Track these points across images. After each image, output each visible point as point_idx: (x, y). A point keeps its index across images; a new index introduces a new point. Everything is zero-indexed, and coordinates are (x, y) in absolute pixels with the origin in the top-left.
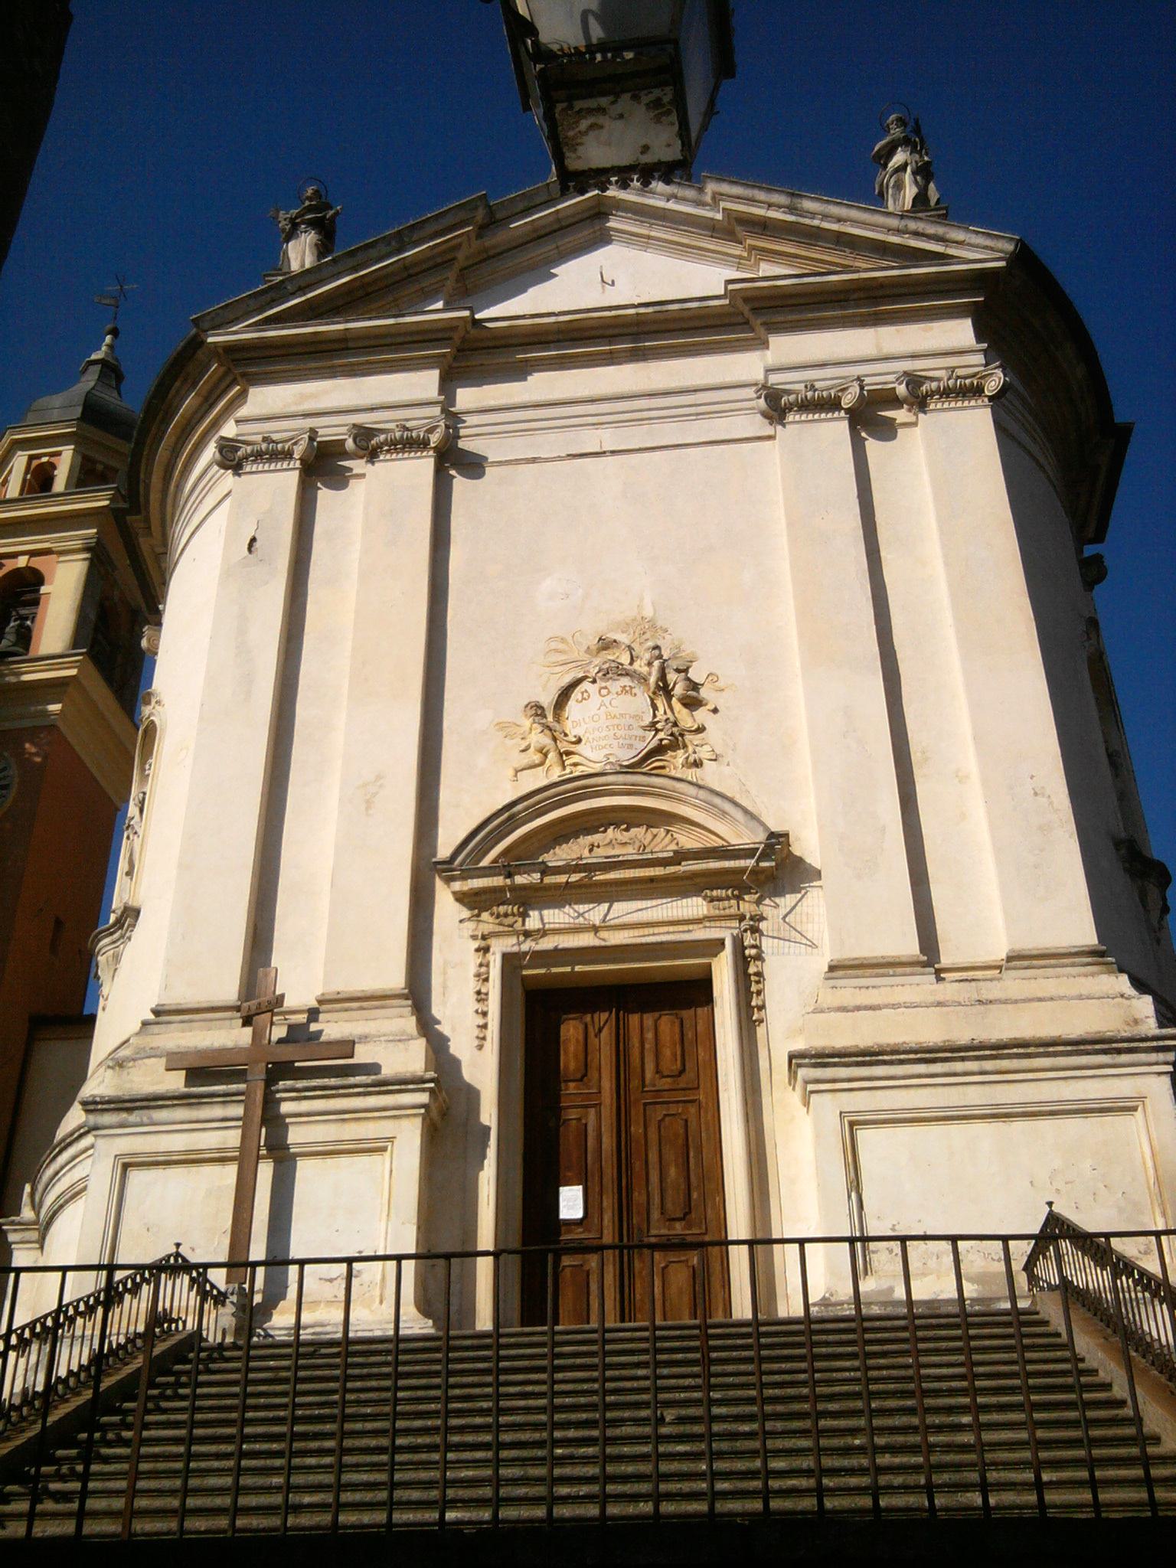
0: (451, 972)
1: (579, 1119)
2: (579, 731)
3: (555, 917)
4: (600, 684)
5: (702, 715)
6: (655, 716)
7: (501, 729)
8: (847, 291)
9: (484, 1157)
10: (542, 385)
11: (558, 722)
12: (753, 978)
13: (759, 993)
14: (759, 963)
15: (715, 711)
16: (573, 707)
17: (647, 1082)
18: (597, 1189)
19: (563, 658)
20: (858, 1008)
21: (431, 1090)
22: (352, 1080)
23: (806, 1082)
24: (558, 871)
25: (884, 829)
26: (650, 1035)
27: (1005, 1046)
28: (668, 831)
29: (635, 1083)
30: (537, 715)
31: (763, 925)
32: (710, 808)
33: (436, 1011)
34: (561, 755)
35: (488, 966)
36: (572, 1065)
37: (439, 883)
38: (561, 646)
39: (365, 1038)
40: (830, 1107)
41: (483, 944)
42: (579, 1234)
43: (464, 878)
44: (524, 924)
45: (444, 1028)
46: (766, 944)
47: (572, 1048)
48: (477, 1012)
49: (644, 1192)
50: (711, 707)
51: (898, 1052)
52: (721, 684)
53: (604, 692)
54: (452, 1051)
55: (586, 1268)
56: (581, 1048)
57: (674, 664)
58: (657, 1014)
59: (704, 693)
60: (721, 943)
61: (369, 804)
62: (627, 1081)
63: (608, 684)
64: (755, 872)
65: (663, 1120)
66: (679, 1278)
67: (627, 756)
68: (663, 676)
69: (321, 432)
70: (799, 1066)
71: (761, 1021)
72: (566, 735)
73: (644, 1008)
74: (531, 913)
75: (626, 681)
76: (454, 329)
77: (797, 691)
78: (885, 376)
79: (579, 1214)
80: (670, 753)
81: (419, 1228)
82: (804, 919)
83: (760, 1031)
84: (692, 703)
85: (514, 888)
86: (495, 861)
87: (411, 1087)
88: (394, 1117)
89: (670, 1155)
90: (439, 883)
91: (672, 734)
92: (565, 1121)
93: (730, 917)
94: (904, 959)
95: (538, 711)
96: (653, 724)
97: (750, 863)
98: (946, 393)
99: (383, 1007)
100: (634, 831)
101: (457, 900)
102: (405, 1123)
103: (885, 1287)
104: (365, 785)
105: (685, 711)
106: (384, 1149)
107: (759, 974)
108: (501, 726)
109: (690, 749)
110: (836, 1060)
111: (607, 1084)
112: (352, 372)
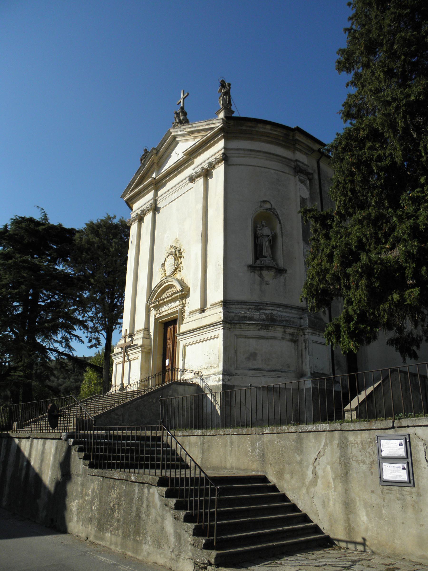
8: (201, 144)
10: (170, 185)
27: (205, 326)
69: (204, 167)
76: (152, 182)
78: (205, 165)
98: (216, 164)
112: (144, 196)
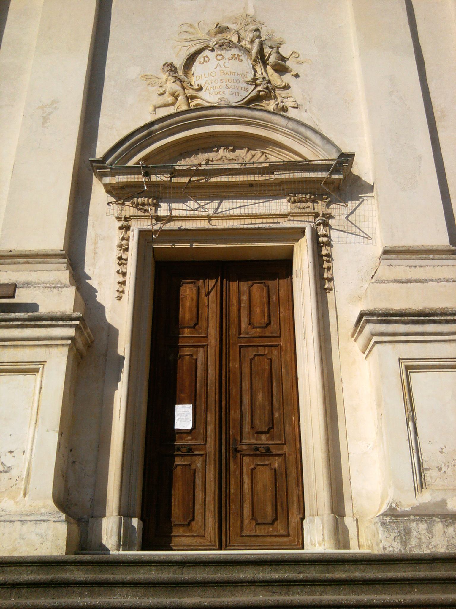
0: (99, 242)
1: (192, 355)
2: (202, 83)
3: (180, 208)
4: (217, 52)
5: (287, 78)
6: (255, 75)
7: (146, 79)
9: (118, 379)
11: (186, 76)
12: (324, 258)
13: (329, 269)
14: (329, 248)
15: (297, 76)
16: (197, 67)
17: (243, 330)
18: (203, 407)
19: (190, 37)
20: (409, 281)
21: (77, 326)
22: (12, 315)
23: (373, 335)
24: (182, 173)
25: (420, 158)
26: (245, 298)
28: (263, 153)
29: (233, 331)
30: (171, 71)
31: (331, 222)
32: (296, 135)
33: (88, 270)
34: (187, 98)
35: (128, 240)
36: (187, 316)
37: (95, 179)
38: (189, 29)
39: (27, 285)
40: (390, 355)
41: (125, 223)
42: (188, 441)
43: (113, 175)
44: (156, 211)
45: (93, 283)
46: (334, 235)
47: (187, 304)
48: (118, 272)
49: (238, 411)
50: (294, 73)
51: (446, 314)
52: (301, 59)
53: (219, 57)
54: (98, 299)
55: (193, 467)
56: (194, 304)
57: (269, 43)
58: (250, 283)
59: (289, 64)
60: (302, 231)
61: (45, 120)
62: (228, 329)
63: (223, 52)
64: (328, 182)
65: (254, 358)
66: (264, 477)
67: (234, 100)
68: (261, 51)
70: (368, 322)
71: (331, 289)
72: (191, 85)
73: (240, 278)
74: (162, 205)
75: (235, 51)
77: (356, 67)
79: (189, 426)
80: (265, 102)
81: (61, 434)
82: (362, 219)
83: (330, 296)
84: (281, 69)
85: (152, 185)
86: (137, 163)
87: (61, 323)
88: (46, 346)
89: (258, 385)
90: (95, 179)
91: (267, 88)
92: (181, 356)
93: (308, 214)
94: (439, 248)
95: (171, 68)
96: (254, 80)
97: (324, 175)
99: (44, 263)
100: (238, 152)
101: (108, 192)
102: (54, 350)
103: (439, 499)
104: (43, 107)
105: (276, 75)
106: (37, 371)
107: (329, 255)
108: (146, 78)
109: (279, 100)
110: (398, 318)
111: (213, 331)
